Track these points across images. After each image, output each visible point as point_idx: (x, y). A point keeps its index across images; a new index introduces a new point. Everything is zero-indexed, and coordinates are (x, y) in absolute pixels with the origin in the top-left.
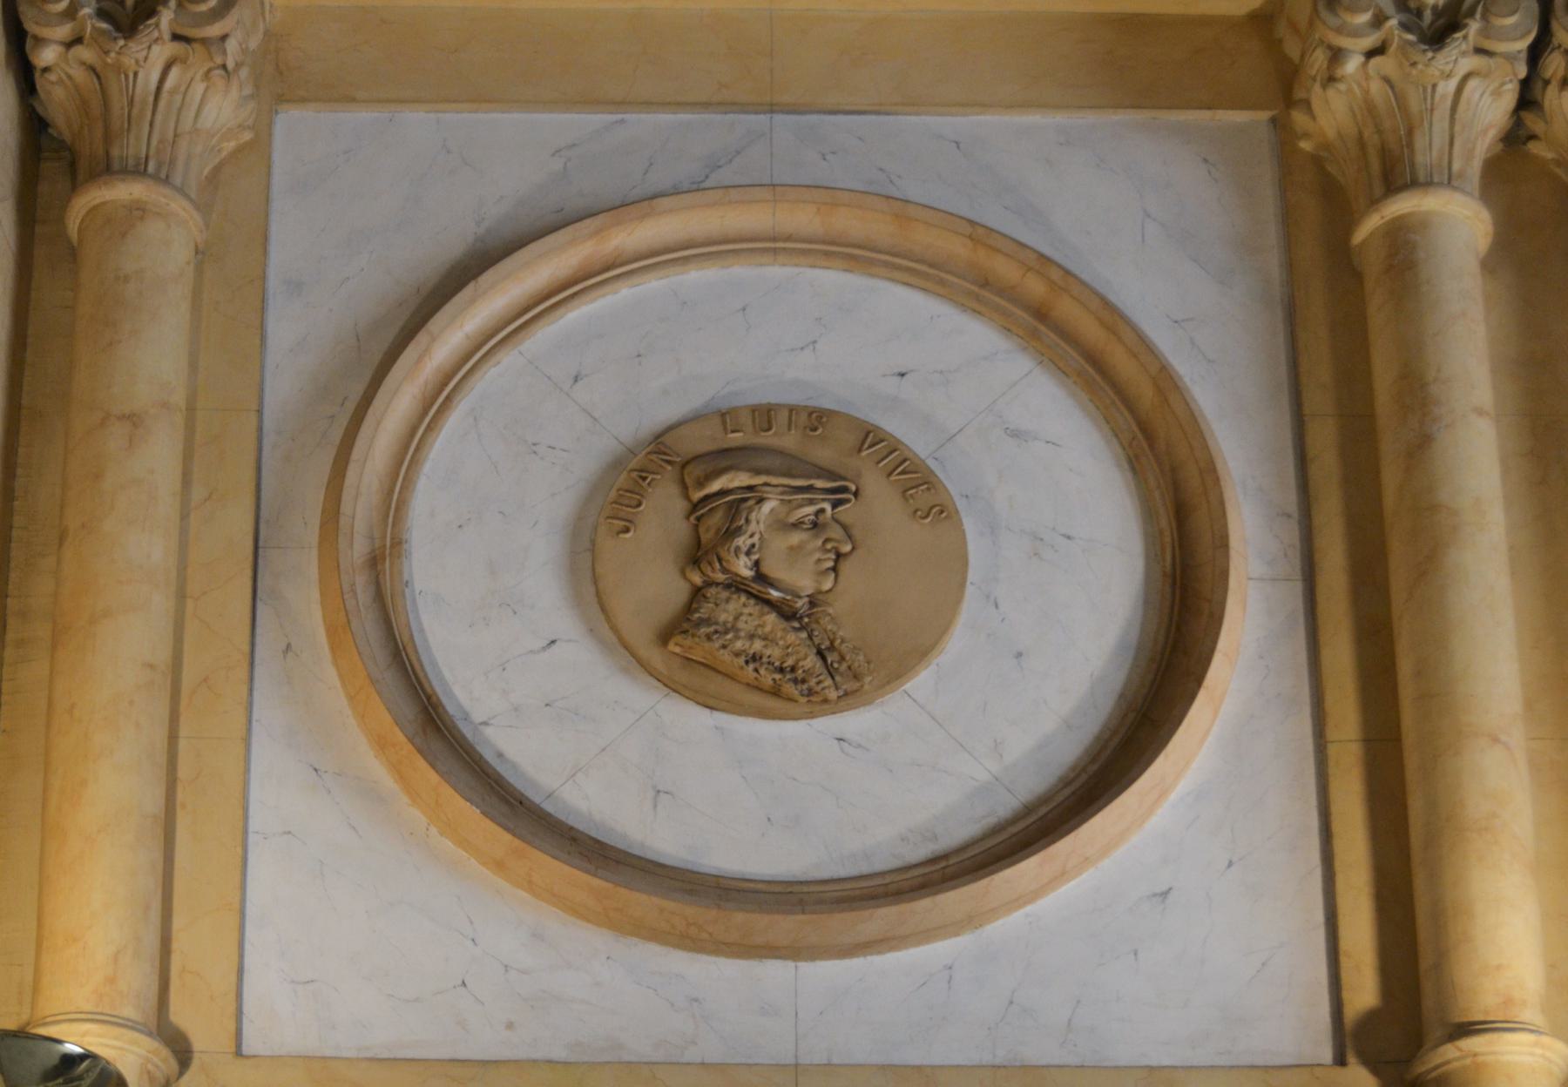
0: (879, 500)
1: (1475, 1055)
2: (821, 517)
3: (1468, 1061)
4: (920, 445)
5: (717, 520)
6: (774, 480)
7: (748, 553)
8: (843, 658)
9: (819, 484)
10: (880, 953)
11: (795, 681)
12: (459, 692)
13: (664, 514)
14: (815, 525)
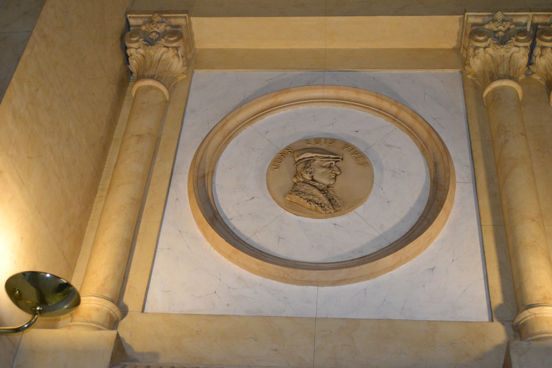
0: (349, 162)
1: (535, 314)
2: (332, 165)
3: (533, 316)
4: (362, 148)
5: (302, 165)
6: (319, 155)
7: (310, 173)
8: (336, 202)
9: (331, 156)
10: (344, 284)
11: (322, 207)
12: (224, 211)
13: (288, 165)
14: (330, 167)
